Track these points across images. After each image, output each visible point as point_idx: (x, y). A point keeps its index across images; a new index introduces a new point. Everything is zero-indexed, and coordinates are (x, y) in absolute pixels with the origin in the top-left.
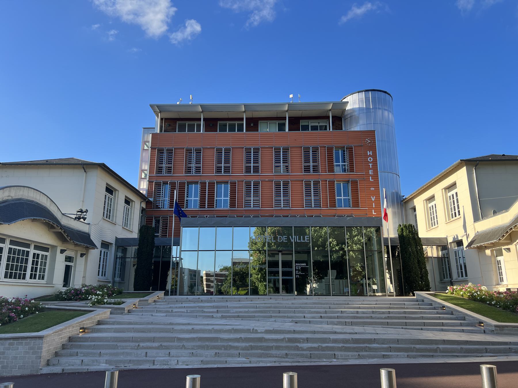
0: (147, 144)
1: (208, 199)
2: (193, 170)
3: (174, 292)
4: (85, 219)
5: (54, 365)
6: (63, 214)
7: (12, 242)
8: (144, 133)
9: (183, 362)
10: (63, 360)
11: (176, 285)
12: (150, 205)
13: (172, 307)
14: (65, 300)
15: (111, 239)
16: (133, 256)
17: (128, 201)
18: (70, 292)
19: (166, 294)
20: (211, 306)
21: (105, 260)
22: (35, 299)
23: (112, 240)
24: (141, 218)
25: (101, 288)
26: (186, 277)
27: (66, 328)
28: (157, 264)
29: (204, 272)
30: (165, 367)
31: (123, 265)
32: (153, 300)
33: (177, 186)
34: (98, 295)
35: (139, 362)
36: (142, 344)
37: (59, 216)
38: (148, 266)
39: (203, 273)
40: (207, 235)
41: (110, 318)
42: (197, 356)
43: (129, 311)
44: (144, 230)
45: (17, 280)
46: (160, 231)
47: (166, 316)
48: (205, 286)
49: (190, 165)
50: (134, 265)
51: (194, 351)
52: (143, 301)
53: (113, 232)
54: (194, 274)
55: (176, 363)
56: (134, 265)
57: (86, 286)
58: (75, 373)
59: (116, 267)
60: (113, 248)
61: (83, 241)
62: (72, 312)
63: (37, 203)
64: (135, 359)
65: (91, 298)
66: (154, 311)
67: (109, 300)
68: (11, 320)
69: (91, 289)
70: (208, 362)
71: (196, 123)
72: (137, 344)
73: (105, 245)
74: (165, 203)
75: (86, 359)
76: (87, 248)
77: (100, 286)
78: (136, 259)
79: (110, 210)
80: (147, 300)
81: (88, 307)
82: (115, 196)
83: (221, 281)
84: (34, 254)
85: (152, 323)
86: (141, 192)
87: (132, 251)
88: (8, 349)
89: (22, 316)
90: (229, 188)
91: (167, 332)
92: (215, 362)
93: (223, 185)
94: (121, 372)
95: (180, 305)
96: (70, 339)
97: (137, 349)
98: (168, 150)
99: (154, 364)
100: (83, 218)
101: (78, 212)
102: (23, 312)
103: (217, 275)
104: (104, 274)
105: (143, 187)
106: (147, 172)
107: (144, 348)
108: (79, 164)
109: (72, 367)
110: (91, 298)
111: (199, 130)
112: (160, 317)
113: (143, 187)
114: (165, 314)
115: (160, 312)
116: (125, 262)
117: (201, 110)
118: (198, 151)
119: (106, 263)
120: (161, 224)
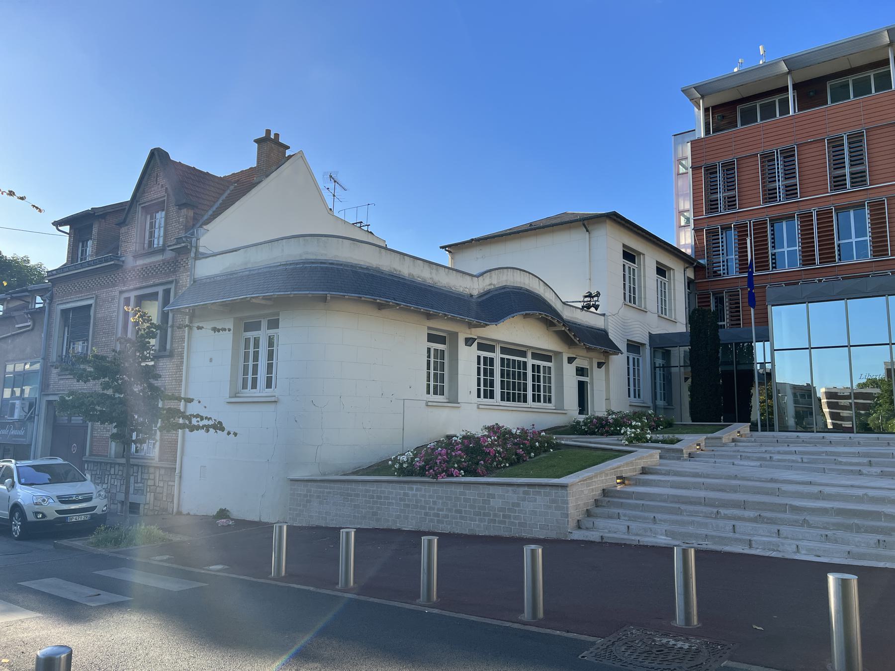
0: (684, 162)
1: (820, 244)
2: (781, 194)
3: (767, 426)
4: (596, 307)
5: (587, 529)
6: (564, 303)
7: (504, 350)
8: (676, 145)
9: (810, 551)
10: (600, 523)
11: (772, 413)
12: (701, 271)
13: (770, 452)
14: (585, 433)
15: (642, 337)
16: (682, 364)
17: (661, 271)
18: (591, 421)
19: (754, 428)
20: (854, 453)
21: (636, 372)
22: (544, 431)
23: (644, 339)
24: (689, 297)
25: (637, 416)
26: (789, 400)
27: (596, 476)
28: (727, 376)
29: (823, 390)
30: (774, 554)
31: (668, 379)
32: (731, 437)
33: (751, 230)
34: (635, 427)
35: (722, 540)
36: (723, 511)
37: (558, 306)
38: (712, 377)
39: (821, 392)
40: (827, 316)
41: (660, 465)
42: (836, 541)
43: (691, 456)
44: (695, 317)
45: (516, 404)
46: (726, 316)
47: (761, 466)
48: (828, 416)
49: (772, 185)
50: (686, 379)
51: (829, 533)
52: (712, 438)
53: (645, 325)
54: (805, 393)
55: (795, 550)
56: (686, 379)
57: (613, 413)
58: (621, 545)
59: (655, 383)
60: (647, 351)
61: (597, 342)
62: (599, 453)
63: (527, 290)
64: (714, 533)
65: (625, 432)
66: (728, 456)
67: (654, 436)
68: (519, 460)
69: (622, 418)
70: (861, 556)
71: (777, 99)
72: (715, 510)
73: (634, 347)
74: (729, 264)
75: (633, 525)
76: (606, 354)
77: (635, 413)
78: (689, 369)
79: (634, 288)
80: (720, 438)
81: (622, 445)
82: (639, 265)
83: (865, 407)
84: (533, 366)
85: (736, 477)
86: (683, 250)
87: (679, 354)
88: (524, 500)
89: (533, 454)
90: (868, 216)
91: (767, 494)
92: (878, 558)
93: (852, 213)
94: (358, 531)
95: (786, 449)
96: (605, 492)
97: (716, 518)
98: (724, 165)
99: (750, 546)
100: (594, 306)
101: (586, 297)
102: (533, 447)
103: (858, 396)
104: (637, 394)
105: (685, 241)
106: (690, 215)
107: (727, 518)
108: (576, 221)
109: (615, 535)
110: (625, 432)
111: (785, 110)
112: (749, 468)
113: (685, 241)
114: (758, 463)
115: (748, 458)
116: (670, 373)
117: (785, 69)
118: (788, 154)
119: (639, 376)
120: (726, 304)
